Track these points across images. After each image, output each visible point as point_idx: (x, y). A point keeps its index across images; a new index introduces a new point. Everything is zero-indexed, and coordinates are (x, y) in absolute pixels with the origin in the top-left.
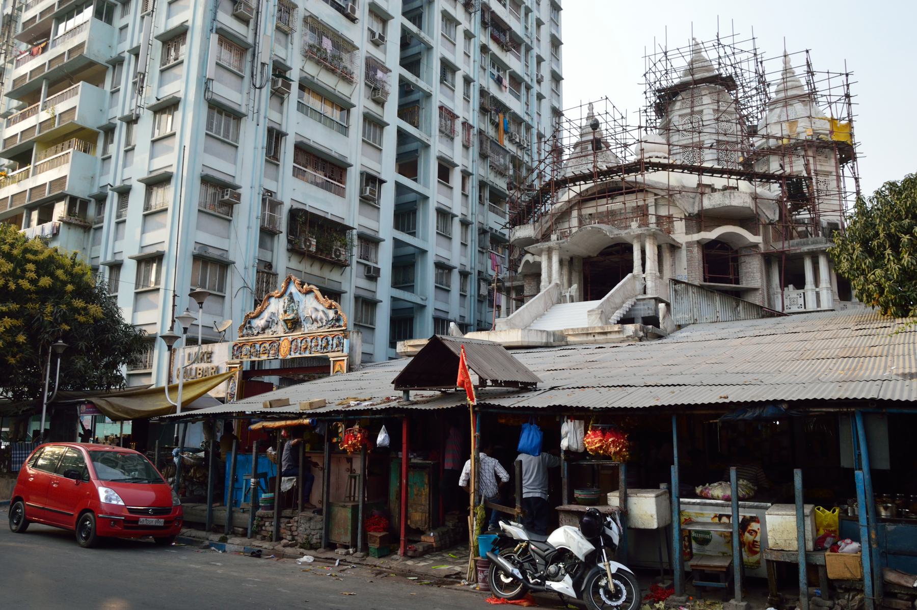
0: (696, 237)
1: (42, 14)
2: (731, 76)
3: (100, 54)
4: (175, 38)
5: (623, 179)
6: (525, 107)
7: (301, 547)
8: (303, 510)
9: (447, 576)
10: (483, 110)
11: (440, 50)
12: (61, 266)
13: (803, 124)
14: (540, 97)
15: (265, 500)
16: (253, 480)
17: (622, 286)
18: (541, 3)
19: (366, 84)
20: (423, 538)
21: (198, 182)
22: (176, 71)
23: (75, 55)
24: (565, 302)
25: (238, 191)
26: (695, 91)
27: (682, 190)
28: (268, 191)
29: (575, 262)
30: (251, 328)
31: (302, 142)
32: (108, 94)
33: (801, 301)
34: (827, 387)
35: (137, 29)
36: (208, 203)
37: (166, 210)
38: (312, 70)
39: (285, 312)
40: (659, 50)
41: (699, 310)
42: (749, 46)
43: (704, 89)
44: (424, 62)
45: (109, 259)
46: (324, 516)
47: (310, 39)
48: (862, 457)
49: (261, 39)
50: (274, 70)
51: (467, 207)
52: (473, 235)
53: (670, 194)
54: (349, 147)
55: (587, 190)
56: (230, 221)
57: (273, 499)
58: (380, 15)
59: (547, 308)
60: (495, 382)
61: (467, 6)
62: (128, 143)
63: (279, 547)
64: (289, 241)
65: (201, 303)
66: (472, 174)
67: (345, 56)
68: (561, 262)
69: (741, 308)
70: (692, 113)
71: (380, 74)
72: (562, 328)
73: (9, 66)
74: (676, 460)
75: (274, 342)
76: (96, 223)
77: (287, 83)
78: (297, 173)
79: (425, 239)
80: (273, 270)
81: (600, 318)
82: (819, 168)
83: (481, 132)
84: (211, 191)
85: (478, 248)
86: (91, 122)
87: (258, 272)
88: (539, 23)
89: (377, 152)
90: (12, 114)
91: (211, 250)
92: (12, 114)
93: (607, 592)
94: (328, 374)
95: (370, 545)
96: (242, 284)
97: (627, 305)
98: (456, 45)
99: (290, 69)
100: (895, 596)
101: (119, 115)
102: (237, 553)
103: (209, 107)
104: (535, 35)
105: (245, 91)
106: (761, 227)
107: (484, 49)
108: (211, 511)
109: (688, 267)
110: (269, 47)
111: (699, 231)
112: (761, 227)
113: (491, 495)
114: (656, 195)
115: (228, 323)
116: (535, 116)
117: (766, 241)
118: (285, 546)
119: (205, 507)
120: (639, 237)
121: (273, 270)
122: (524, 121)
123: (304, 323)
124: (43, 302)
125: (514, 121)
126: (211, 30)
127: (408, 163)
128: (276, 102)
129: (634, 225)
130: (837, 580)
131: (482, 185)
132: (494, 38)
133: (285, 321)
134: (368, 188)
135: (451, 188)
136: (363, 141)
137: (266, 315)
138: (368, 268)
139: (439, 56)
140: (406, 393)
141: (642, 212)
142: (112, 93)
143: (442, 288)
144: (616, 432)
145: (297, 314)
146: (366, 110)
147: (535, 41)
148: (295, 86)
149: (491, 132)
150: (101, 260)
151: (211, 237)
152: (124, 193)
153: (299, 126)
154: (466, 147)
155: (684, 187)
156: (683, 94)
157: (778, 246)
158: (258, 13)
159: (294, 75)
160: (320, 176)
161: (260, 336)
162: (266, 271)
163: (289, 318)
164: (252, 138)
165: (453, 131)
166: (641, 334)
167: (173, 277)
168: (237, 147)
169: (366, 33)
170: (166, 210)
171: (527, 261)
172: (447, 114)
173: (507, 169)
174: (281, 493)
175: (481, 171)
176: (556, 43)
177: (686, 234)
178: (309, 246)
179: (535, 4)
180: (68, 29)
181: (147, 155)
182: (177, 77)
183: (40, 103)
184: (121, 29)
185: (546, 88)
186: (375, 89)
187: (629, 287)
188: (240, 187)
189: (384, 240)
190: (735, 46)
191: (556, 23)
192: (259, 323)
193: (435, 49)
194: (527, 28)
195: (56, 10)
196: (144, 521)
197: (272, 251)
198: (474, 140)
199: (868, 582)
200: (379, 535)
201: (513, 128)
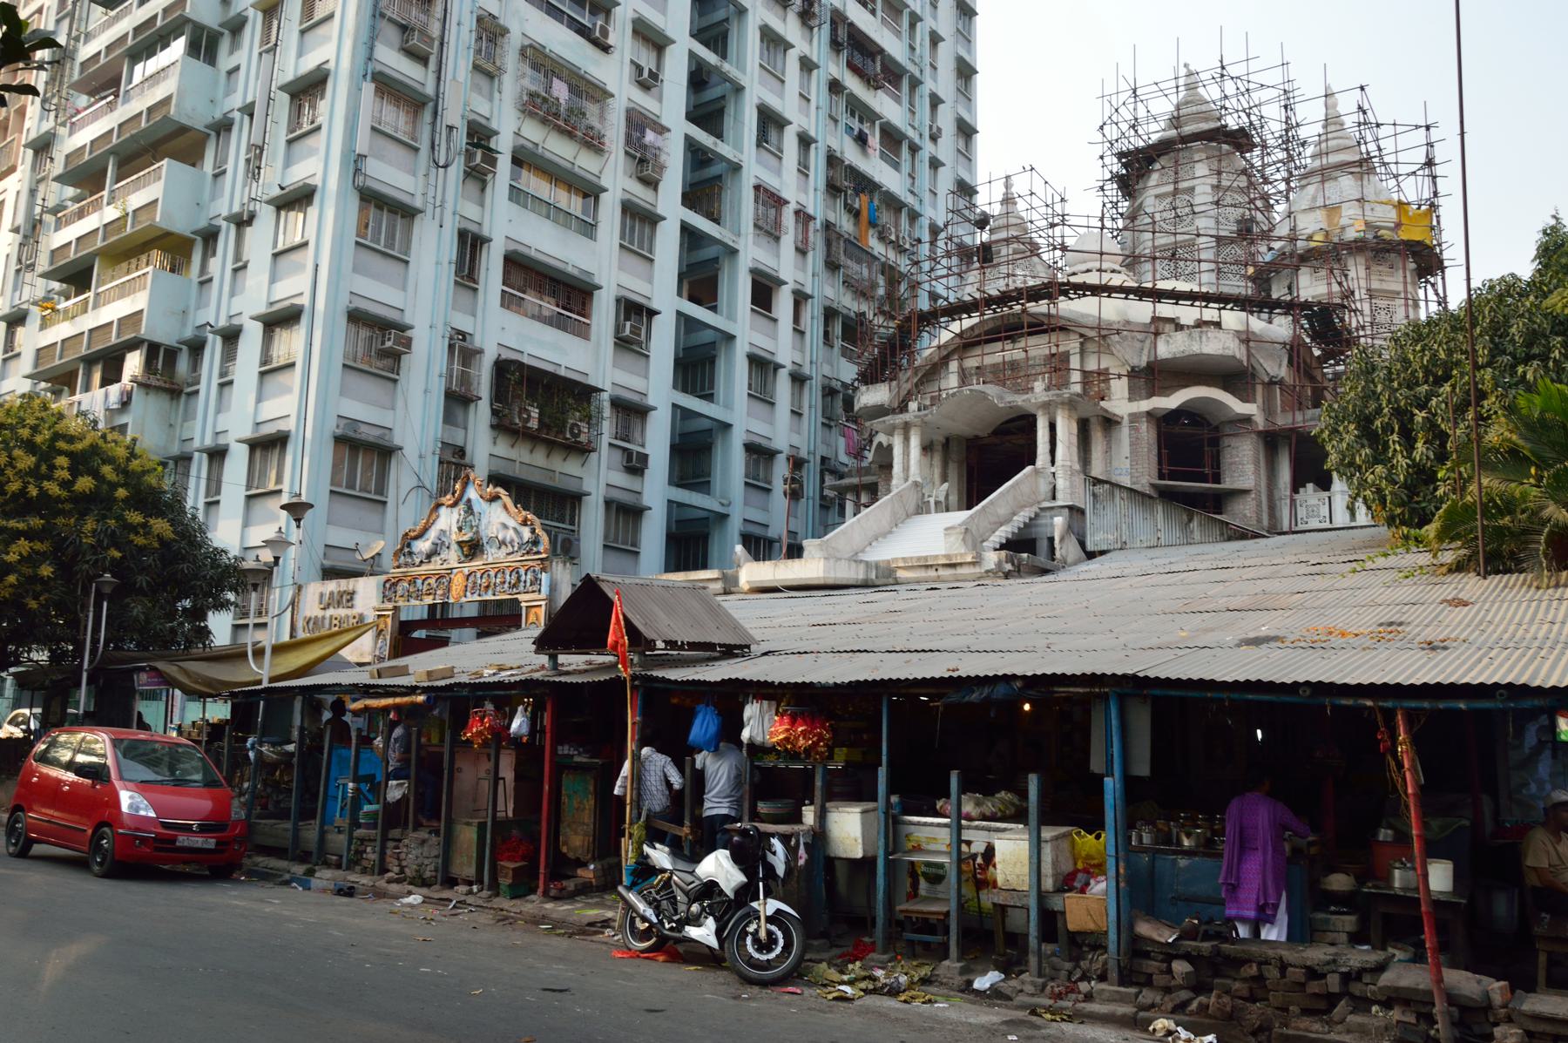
0: (1145, 405)
1: (109, 48)
2: (1242, 130)
3: (196, 114)
4: (309, 88)
5: (1024, 311)
6: (909, 181)
7: (410, 884)
8: (415, 830)
9: (591, 924)
10: (833, 189)
11: (757, 90)
12: (109, 460)
13: (1351, 212)
14: (935, 164)
15: (367, 814)
16: (351, 785)
17: (1008, 491)
18: (939, 5)
19: (627, 153)
20: (580, 872)
21: (343, 321)
22: (310, 141)
23: (157, 117)
24: (928, 512)
25: (409, 333)
26: (1186, 154)
27: (1125, 328)
28: (459, 332)
29: (954, 447)
30: (410, 553)
31: (515, 252)
32: (209, 178)
33: (1325, 511)
34: (1511, 655)
35: (253, 73)
36: (360, 355)
37: (292, 365)
38: (534, 133)
39: (460, 529)
40: (1123, 86)
41: (1131, 526)
42: (1275, 77)
43: (1198, 150)
44: (730, 110)
45: (208, 442)
46: (441, 839)
47: (532, 81)
48: (1116, 754)
49: (448, 88)
50: (469, 135)
51: (802, 351)
52: (812, 397)
53: (1100, 336)
54: (599, 258)
55: (972, 328)
56: (395, 381)
57: (376, 813)
58: (651, 38)
59: (896, 523)
60: (671, 644)
61: (806, 16)
62: (237, 258)
63: (381, 883)
64: (494, 412)
65: (298, 520)
66: (811, 297)
67: (592, 109)
68: (927, 448)
69: (1195, 524)
70: (1176, 192)
71: (650, 137)
72: (889, 557)
73: (63, 131)
74: (884, 758)
75: (442, 577)
76: (190, 385)
77: (491, 157)
78: (507, 301)
79: (728, 406)
80: (467, 460)
81: (964, 540)
82: (1375, 285)
83: (828, 226)
84: (364, 333)
85: (820, 419)
86: (182, 224)
87: (441, 462)
88: (935, 39)
89: (647, 264)
90: (65, 208)
91: (363, 428)
92: (65, 208)
93: (756, 940)
94: (518, 626)
95: (501, 880)
96: (415, 482)
97: (1021, 518)
98: (787, 82)
99: (496, 133)
100: (1147, 955)
101: (225, 213)
102: (324, 890)
103: (362, 199)
104: (927, 60)
105: (422, 171)
106: (1259, 388)
107: (835, 87)
108: (296, 830)
109: (1130, 459)
110: (461, 97)
111: (1150, 395)
112: (1259, 388)
113: (658, 809)
114: (1082, 335)
115: (378, 546)
116: (927, 197)
117: (1268, 410)
118: (389, 882)
119: (288, 825)
120: (1047, 406)
121: (467, 460)
122: (904, 205)
123: (487, 547)
124: (82, 515)
125: (888, 206)
126: (365, 76)
127: (701, 279)
128: (473, 187)
129: (1039, 386)
130: (1079, 933)
131: (830, 314)
132: (851, 66)
133: (460, 543)
134: (628, 324)
135: (775, 320)
136: (621, 246)
137: (432, 534)
138: (628, 453)
139: (756, 101)
140: (553, 658)
141: (1058, 365)
142: (216, 176)
143: (757, 485)
144: (810, 719)
145: (477, 532)
146: (628, 196)
147: (928, 69)
148: (504, 164)
149: (846, 224)
150: (197, 444)
151: (364, 408)
152: (231, 336)
153: (510, 225)
154: (802, 251)
155: (1128, 322)
156: (1164, 161)
157: (1283, 421)
158: (442, 44)
159: (504, 144)
160: (550, 307)
161: (424, 567)
162: (454, 463)
163: (466, 538)
164: (432, 248)
165: (777, 224)
166: (1009, 567)
167: (304, 471)
168: (407, 262)
169: (627, 70)
170: (292, 365)
171: (880, 444)
172: (769, 199)
173: (874, 286)
174: (386, 805)
175: (829, 291)
176: (966, 72)
177: (1130, 400)
178: (528, 420)
179: (928, 6)
180: (148, 74)
181: (266, 277)
182: (312, 152)
183: (105, 193)
184: (230, 73)
185: (946, 149)
186: (642, 161)
187: (1025, 488)
188: (411, 328)
189: (654, 409)
190: (1251, 78)
191: (966, 36)
192: (423, 546)
193: (747, 90)
194: (912, 48)
195: (130, 42)
196: (183, 840)
197: (466, 428)
198: (816, 240)
199: (1112, 936)
200: (512, 865)
201: (885, 217)
